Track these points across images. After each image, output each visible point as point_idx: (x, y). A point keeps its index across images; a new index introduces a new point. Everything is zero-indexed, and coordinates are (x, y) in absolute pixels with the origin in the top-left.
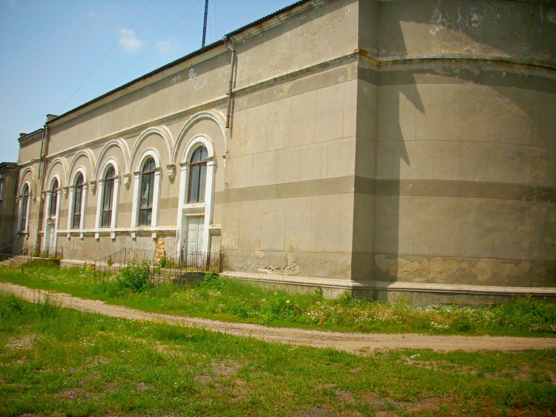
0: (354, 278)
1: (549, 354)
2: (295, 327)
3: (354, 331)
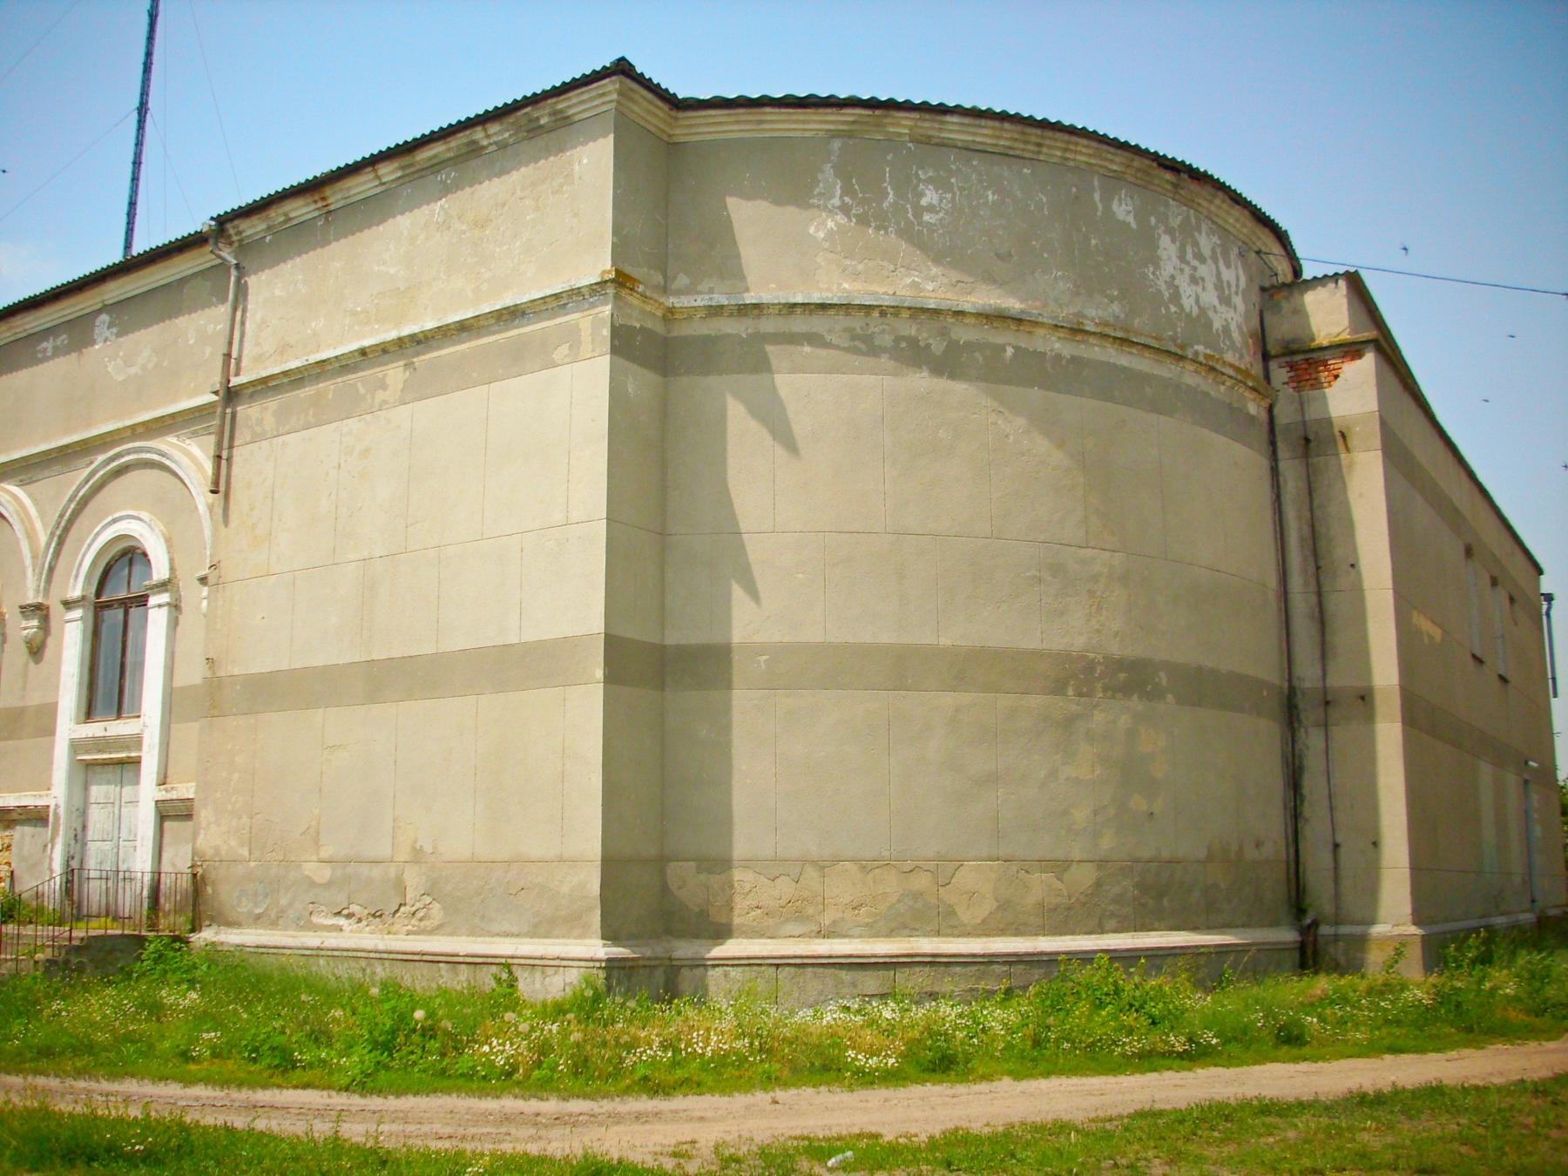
0: (610, 934)
1: (1203, 1120)
2: (447, 1091)
3: (627, 1091)
